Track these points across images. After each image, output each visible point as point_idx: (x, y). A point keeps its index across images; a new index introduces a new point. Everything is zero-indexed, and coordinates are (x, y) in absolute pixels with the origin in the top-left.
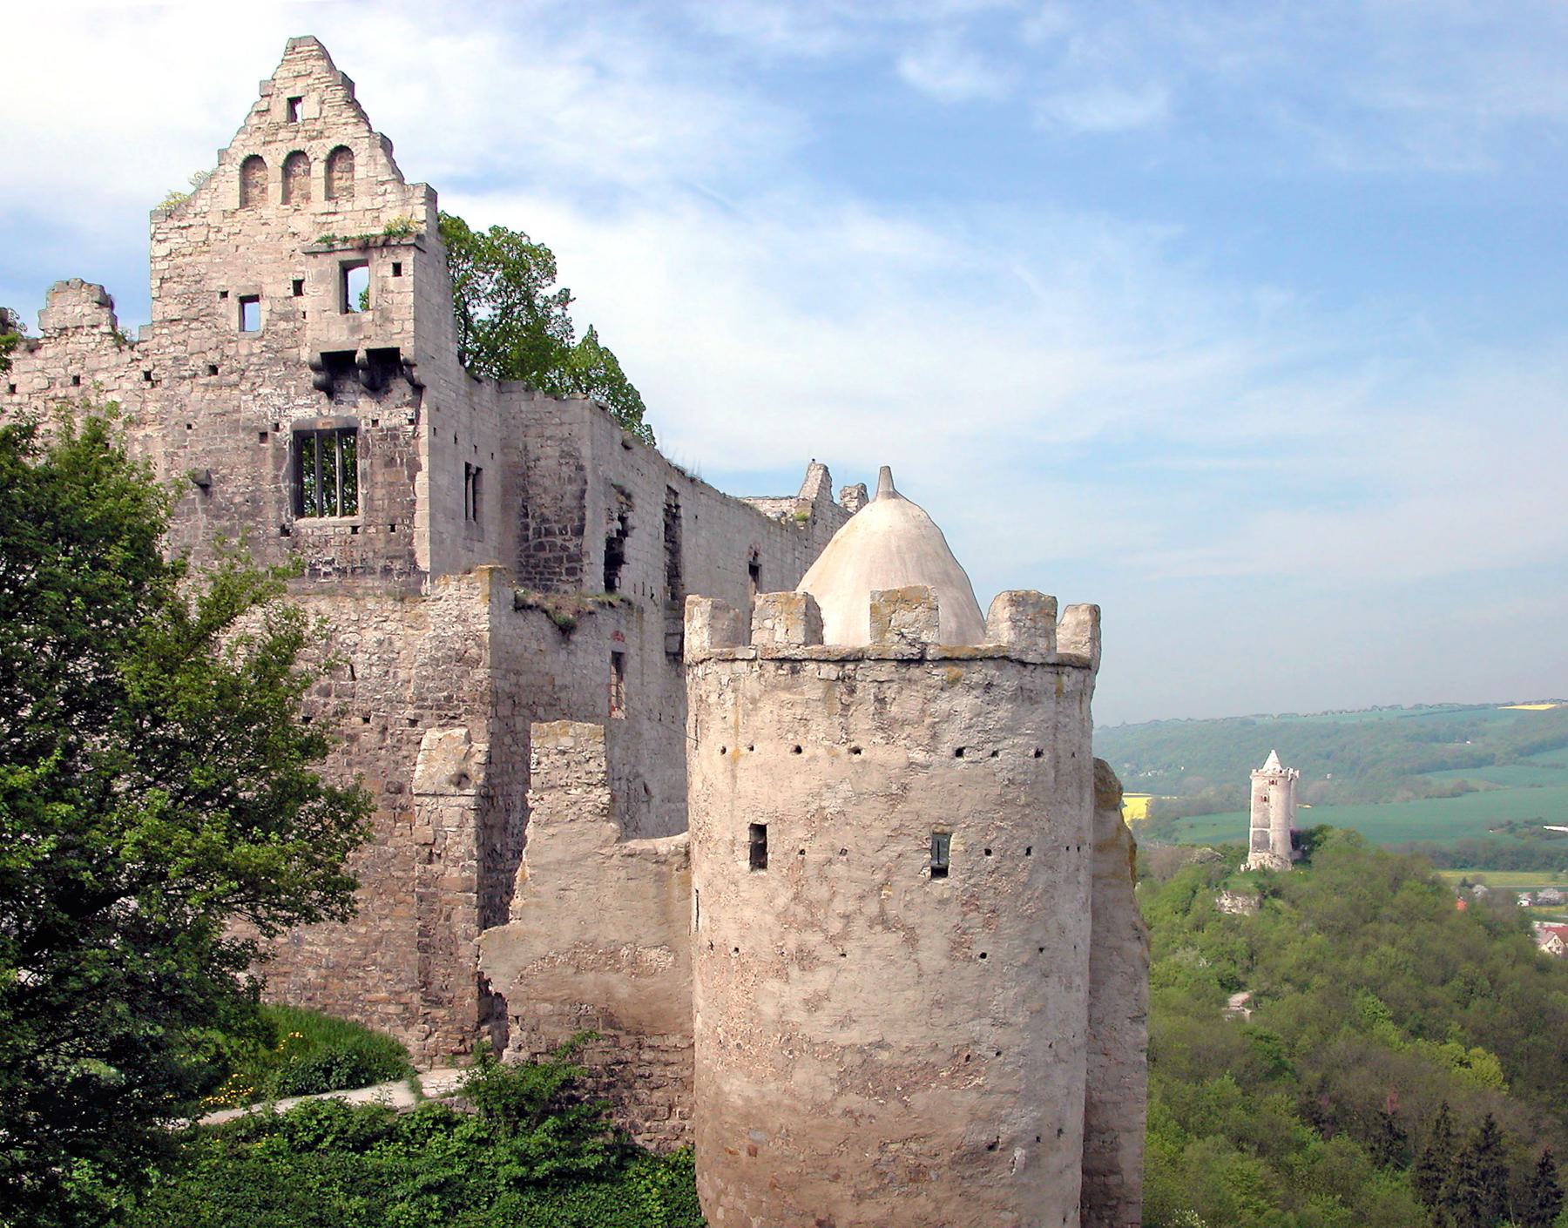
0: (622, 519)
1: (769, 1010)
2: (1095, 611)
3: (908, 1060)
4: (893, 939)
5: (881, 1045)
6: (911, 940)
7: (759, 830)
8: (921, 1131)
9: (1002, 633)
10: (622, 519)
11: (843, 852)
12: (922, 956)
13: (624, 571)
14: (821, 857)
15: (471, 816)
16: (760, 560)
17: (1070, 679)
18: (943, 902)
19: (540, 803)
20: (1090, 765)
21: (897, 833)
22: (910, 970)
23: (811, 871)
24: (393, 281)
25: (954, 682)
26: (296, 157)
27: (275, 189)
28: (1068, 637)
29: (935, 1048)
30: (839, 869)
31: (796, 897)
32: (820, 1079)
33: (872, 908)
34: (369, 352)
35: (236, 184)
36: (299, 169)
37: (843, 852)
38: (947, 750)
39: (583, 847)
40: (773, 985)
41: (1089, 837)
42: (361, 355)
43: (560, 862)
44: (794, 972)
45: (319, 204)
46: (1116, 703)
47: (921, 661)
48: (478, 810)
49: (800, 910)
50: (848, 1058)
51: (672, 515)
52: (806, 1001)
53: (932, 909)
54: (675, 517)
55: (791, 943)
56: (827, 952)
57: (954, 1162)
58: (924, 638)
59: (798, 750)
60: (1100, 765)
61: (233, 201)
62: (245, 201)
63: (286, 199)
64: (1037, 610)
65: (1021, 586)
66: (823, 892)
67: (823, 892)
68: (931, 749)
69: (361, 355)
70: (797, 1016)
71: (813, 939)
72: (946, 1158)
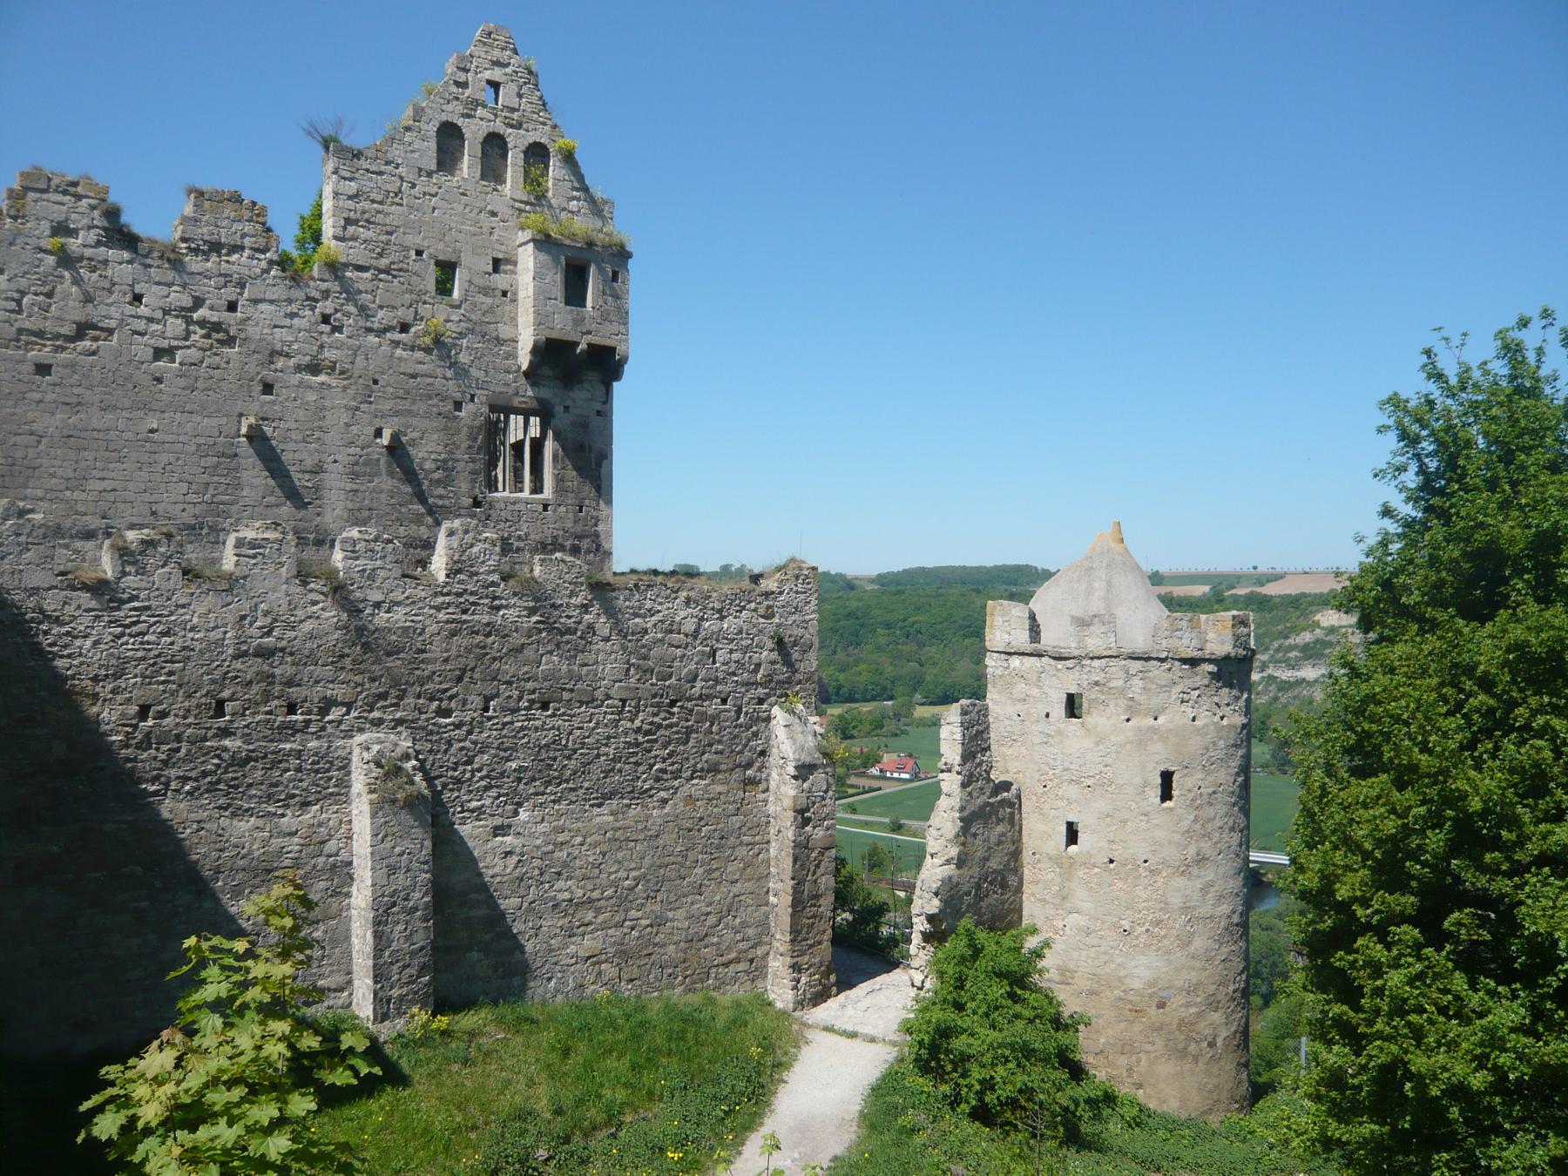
1: (1176, 901)
7: (1167, 777)
23: (1205, 799)
31: (1196, 820)
40: (1180, 882)
44: (1195, 871)
55: (1192, 850)
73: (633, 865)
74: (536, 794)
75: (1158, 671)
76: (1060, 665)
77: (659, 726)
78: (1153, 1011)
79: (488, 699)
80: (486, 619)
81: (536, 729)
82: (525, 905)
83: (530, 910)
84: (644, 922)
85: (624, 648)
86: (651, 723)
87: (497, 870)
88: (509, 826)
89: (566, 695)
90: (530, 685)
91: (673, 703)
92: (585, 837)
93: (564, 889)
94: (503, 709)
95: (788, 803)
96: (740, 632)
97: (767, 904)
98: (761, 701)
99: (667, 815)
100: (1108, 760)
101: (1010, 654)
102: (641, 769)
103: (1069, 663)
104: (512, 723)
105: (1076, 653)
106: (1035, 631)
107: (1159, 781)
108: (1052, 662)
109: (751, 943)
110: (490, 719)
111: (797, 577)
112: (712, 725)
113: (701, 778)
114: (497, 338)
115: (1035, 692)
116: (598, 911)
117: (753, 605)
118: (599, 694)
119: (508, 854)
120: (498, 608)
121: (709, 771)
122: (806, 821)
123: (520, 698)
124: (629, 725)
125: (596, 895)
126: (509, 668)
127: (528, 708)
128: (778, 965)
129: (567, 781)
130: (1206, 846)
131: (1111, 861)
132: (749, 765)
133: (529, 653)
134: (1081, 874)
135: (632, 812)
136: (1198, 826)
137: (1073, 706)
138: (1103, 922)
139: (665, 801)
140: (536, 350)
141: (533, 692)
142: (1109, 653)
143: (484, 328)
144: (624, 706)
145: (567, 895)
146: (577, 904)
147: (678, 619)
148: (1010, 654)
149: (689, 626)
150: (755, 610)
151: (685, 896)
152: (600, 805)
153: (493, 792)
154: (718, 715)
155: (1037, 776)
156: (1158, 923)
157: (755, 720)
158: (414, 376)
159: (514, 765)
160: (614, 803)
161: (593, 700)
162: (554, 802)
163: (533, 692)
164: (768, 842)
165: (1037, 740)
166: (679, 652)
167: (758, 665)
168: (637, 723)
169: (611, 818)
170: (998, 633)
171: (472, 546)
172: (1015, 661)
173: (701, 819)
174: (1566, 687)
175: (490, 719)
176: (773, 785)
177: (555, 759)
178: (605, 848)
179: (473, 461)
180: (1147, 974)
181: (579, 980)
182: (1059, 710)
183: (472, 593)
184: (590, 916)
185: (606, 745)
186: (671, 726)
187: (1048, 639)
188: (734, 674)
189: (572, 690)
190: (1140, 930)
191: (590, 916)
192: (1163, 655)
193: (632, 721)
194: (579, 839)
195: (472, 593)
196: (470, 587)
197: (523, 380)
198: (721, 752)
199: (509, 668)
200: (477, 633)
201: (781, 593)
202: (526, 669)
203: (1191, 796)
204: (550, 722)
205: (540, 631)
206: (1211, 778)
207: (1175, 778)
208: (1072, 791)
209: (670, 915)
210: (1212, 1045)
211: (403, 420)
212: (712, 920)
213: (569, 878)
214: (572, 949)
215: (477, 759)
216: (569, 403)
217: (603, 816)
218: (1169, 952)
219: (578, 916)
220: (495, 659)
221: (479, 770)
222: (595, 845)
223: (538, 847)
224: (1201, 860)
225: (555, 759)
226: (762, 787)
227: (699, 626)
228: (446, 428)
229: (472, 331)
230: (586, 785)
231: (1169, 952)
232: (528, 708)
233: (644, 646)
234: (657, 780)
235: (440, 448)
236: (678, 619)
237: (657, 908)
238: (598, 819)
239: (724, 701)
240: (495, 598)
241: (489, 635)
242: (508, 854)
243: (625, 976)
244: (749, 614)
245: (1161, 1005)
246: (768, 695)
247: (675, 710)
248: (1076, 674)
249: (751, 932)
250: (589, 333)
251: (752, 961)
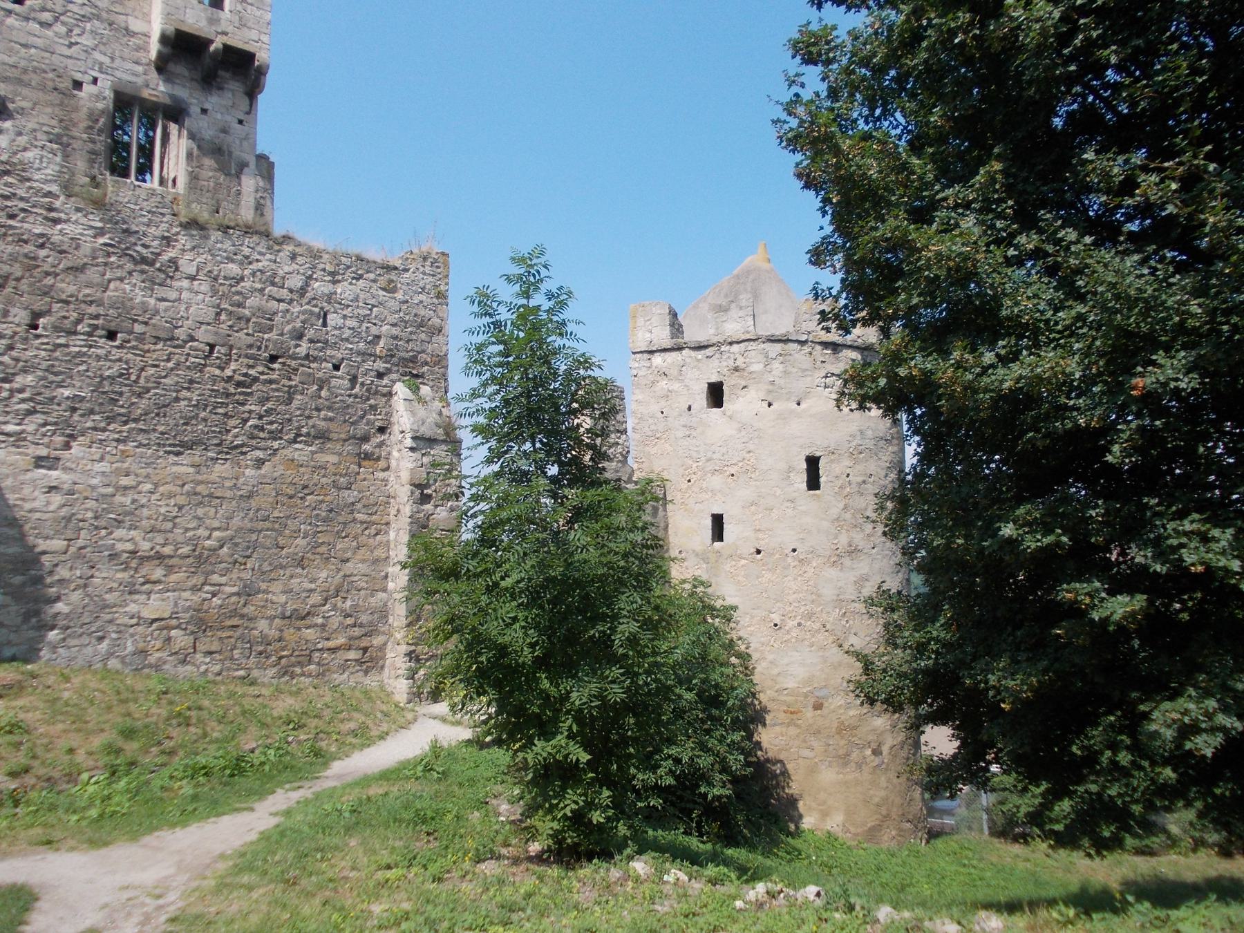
1: (828, 592)
7: (813, 463)
14: (860, 479)
23: (855, 488)
31: (845, 508)
40: (832, 573)
44: (847, 561)
55: (843, 540)
73: (216, 524)
74: (95, 429)
75: (800, 355)
76: (700, 355)
77: (256, 379)
78: (809, 713)
79: (36, 315)
80: (38, 230)
81: (98, 358)
82: (72, 550)
83: (79, 555)
84: (228, 589)
85: (215, 292)
86: (246, 375)
87: (36, 504)
88: (58, 459)
89: (138, 328)
90: (92, 309)
91: (273, 359)
92: (156, 485)
93: (123, 539)
94: (57, 329)
95: (405, 476)
96: (356, 299)
97: (385, 590)
98: (380, 375)
99: (264, 476)
100: (751, 447)
101: (652, 352)
102: (232, 422)
103: (709, 352)
104: (67, 346)
105: (715, 340)
106: (676, 327)
107: (805, 466)
108: (693, 353)
109: (363, 631)
110: (38, 337)
111: (425, 259)
112: (321, 388)
113: (306, 443)
114: (127, 29)
115: (676, 386)
116: (170, 569)
117: (372, 276)
118: (181, 333)
119: (52, 489)
120: (56, 221)
121: (315, 437)
122: (425, 499)
123: (79, 321)
124: (217, 372)
125: (167, 550)
126: (67, 287)
127: (90, 334)
128: (396, 657)
129: (136, 420)
130: (858, 538)
131: (759, 552)
132: (365, 439)
133: (92, 274)
134: (727, 567)
135: (218, 468)
136: (848, 516)
137: (716, 394)
138: (752, 617)
139: (260, 463)
140: (164, 39)
141: (97, 317)
142: (748, 336)
143: (113, 17)
144: (211, 351)
145: (129, 546)
146: (142, 558)
147: (281, 273)
148: (652, 352)
149: (296, 282)
150: (374, 281)
151: (283, 567)
152: (178, 454)
153: (39, 418)
154: (327, 381)
155: (681, 471)
156: (810, 616)
157: (371, 392)
158: (25, 46)
159: (67, 393)
160: (196, 455)
161: (172, 339)
162: (118, 441)
163: (97, 317)
164: (387, 524)
165: (680, 434)
166: (283, 306)
167: (379, 337)
168: (228, 372)
169: (191, 470)
170: (640, 334)
171: (25, 149)
172: (658, 359)
173: (305, 487)
174: (1239, 669)
175: (38, 337)
176: (393, 463)
177: (121, 394)
178: (181, 500)
179: (93, 142)
180: (801, 672)
181: (141, 645)
182: (701, 399)
183: (22, 199)
184: (158, 573)
185: (188, 389)
186: (271, 382)
187: (692, 334)
188: (347, 340)
189: (146, 323)
190: (791, 623)
191: (158, 573)
192: (804, 338)
193: (223, 369)
194: (148, 486)
195: (22, 199)
196: (21, 192)
197: (154, 74)
198: (331, 419)
199: (67, 287)
200: (26, 242)
201: (406, 270)
202: (87, 291)
203: (839, 483)
204: (116, 354)
205: (109, 255)
206: (860, 467)
207: (821, 463)
208: (716, 482)
209: (263, 586)
210: (877, 752)
211: (11, 88)
212: (316, 599)
213: (133, 527)
214: (132, 608)
215: (18, 379)
216: (207, 106)
217: (183, 466)
218: (823, 648)
219: (143, 571)
220: (47, 274)
221: (21, 391)
222: (171, 495)
223: (93, 488)
224: (853, 551)
225: (121, 394)
226: (382, 464)
227: (307, 285)
228: (61, 104)
229: (98, 18)
230: (161, 428)
231: (823, 648)
232: (90, 334)
233: (239, 293)
234: (252, 437)
235: (54, 123)
236: (281, 273)
237: (247, 575)
238: (175, 469)
239: (336, 367)
240: (51, 210)
241: (42, 246)
242: (52, 489)
243: (200, 647)
244: (368, 284)
245: (818, 706)
246: (389, 371)
247: (276, 366)
248: (715, 362)
249: (364, 618)
250: (225, 33)
251: (365, 650)
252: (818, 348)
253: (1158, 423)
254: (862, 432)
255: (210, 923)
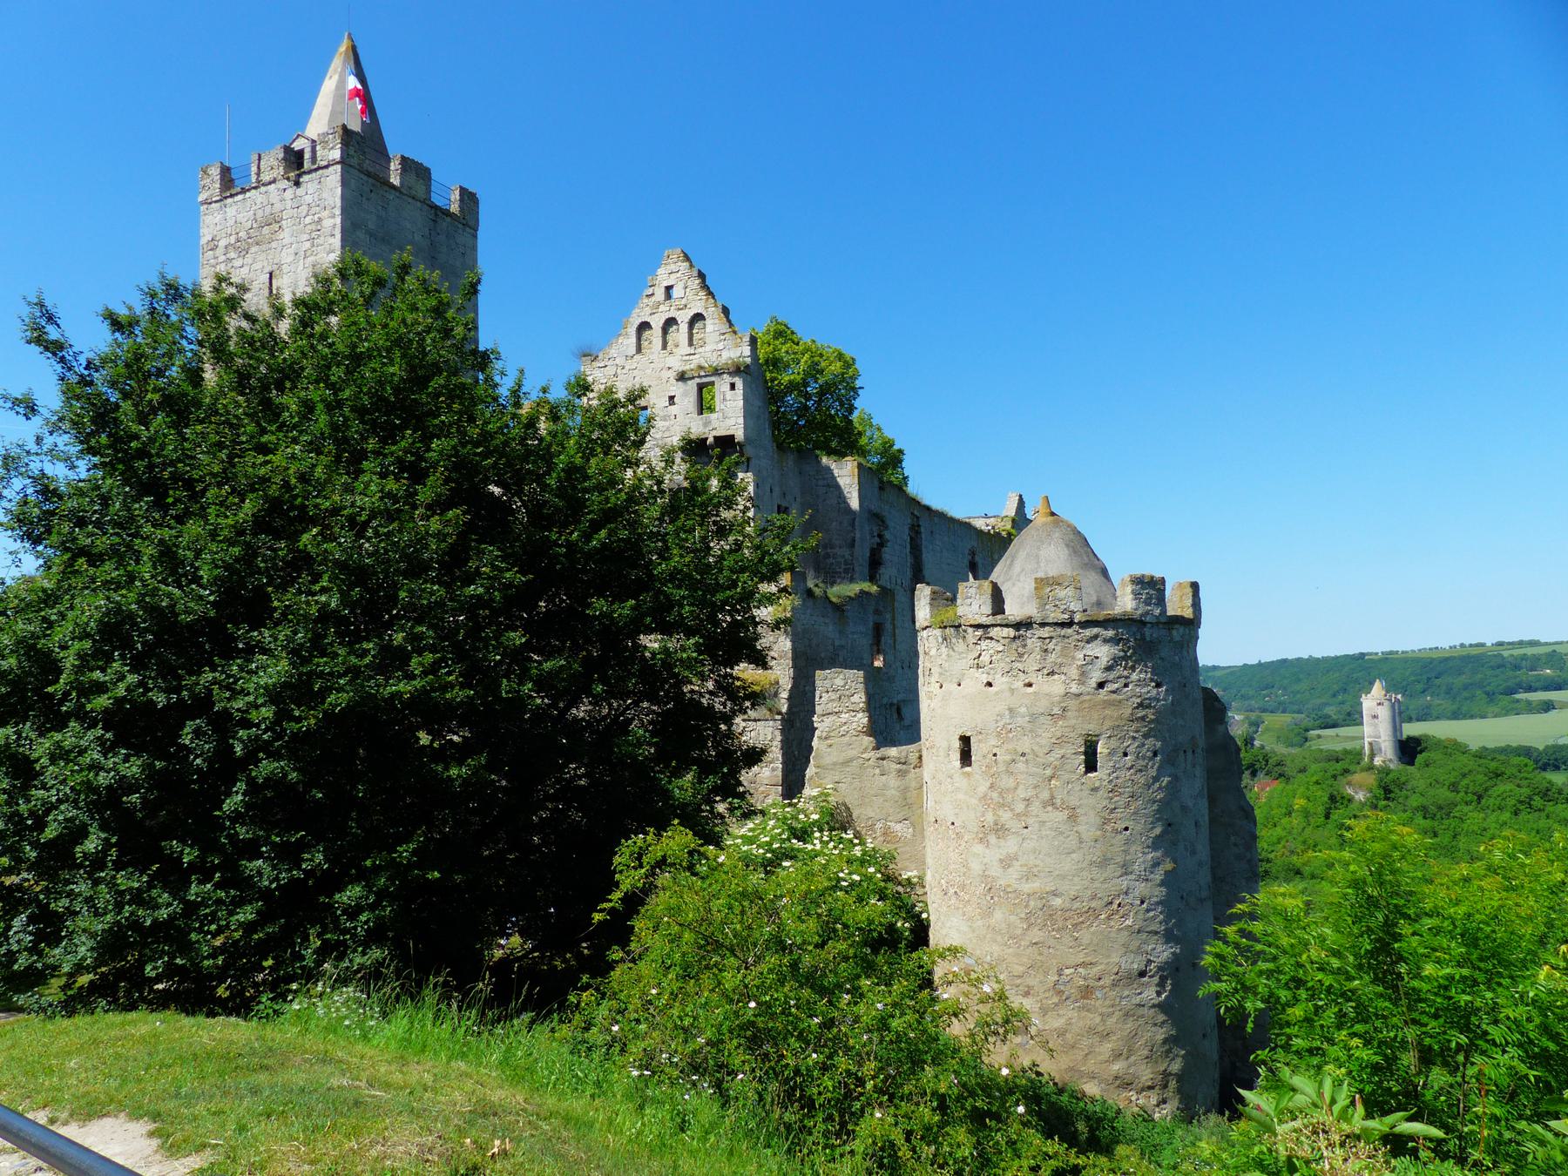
0: (880, 536)
1: (976, 867)
2: (1195, 586)
3: (1077, 905)
4: (1062, 816)
5: (1055, 894)
6: (1073, 818)
7: (965, 740)
8: (1088, 959)
9: (1126, 603)
10: (880, 536)
11: (1023, 755)
12: (1081, 828)
13: (882, 570)
14: (1008, 758)
15: (778, 733)
16: (977, 558)
17: (1177, 633)
18: (1095, 790)
19: (821, 724)
20: (1199, 695)
21: (1060, 741)
22: (1072, 842)
23: (1002, 768)
24: (729, 394)
25: (1096, 637)
26: (670, 322)
27: (658, 342)
28: (1177, 605)
29: (1094, 897)
30: (1021, 766)
31: (992, 786)
32: (1013, 918)
33: (1046, 795)
34: (715, 438)
35: (634, 340)
36: (646, 334)
37: (1023, 755)
38: (1093, 683)
39: (852, 753)
40: (978, 848)
41: (1201, 742)
42: (710, 440)
43: (835, 764)
44: (993, 839)
45: (684, 348)
46: (1216, 649)
47: (1070, 624)
48: (783, 731)
49: (995, 795)
50: (1032, 903)
51: (915, 530)
52: (1001, 861)
53: (1088, 797)
54: (918, 533)
55: (990, 818)
56: (1016, 825)
57: (1114, 985)
58: (1072, 608)
59: (990, 684)
60: (1209, 695)
61: (633, 350)
62: (639, 350)
63: (664, 347)
64: (1151, 587)
65: (1138, 572)
66: (1011, 783)
67: (1011, 783)
68: (1081, 682)
69: (710, 440)
70: (995, 871)
71: (1005, 816)
72: (1107, 981)
136: (995, 795)
207: (972, 740)
252: (970, 630)
253: (458, 878)
254: (1011, 710)
255: (423, 1051)
